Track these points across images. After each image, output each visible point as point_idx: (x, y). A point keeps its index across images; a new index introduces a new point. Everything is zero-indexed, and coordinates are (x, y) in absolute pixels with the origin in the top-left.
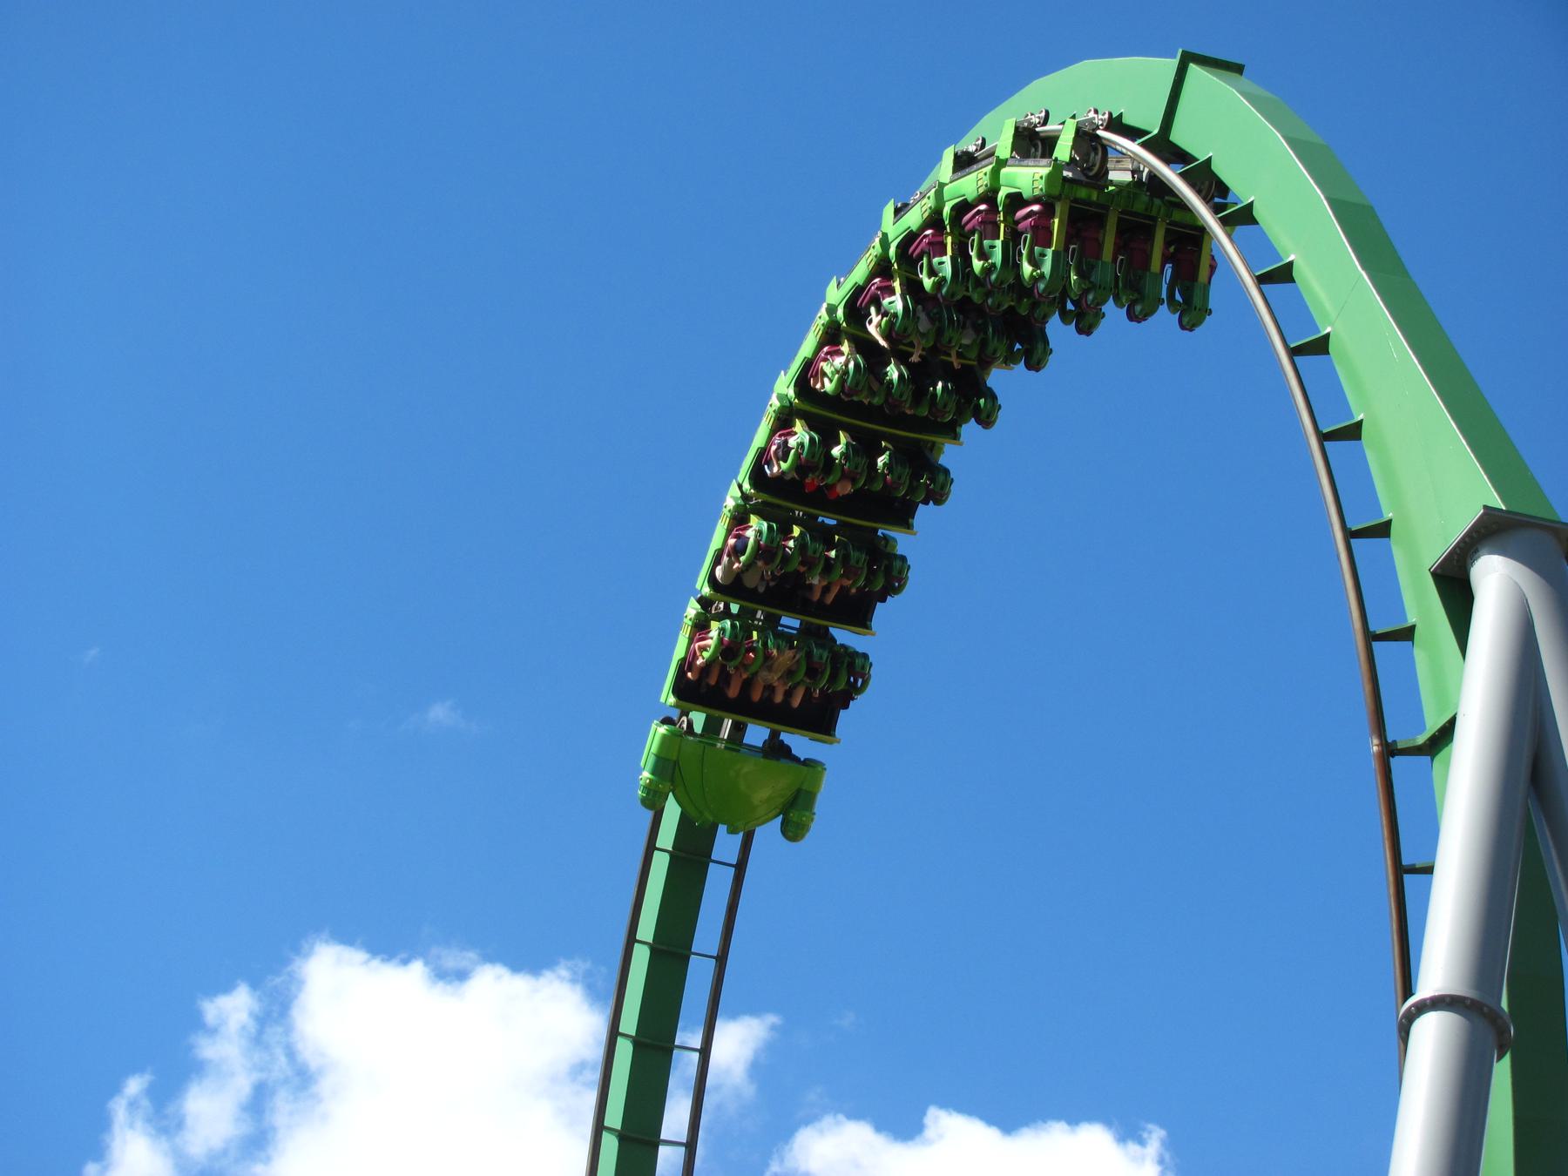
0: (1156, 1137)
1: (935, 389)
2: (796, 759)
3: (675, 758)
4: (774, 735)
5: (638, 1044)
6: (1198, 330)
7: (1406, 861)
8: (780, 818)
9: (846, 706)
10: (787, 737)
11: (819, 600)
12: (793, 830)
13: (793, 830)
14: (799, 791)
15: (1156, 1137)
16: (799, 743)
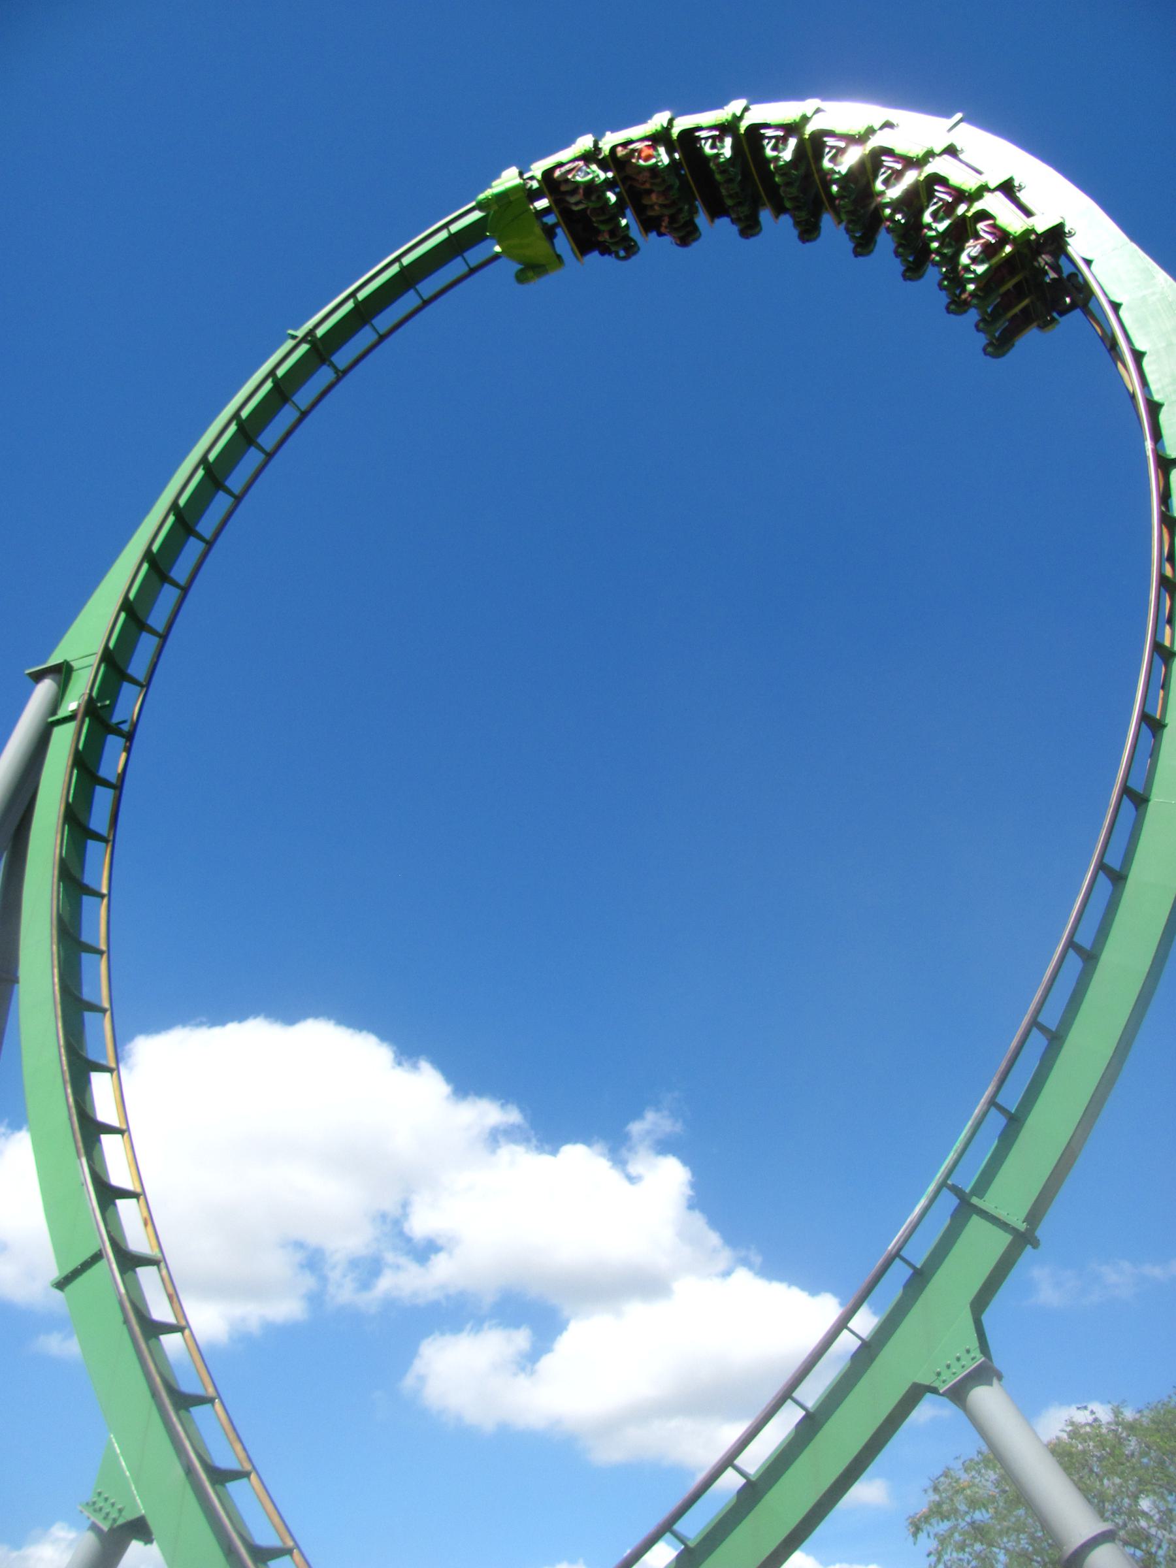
0: (581, 1561)
1: (794, 174)
2: (553, 244)
3: (512, 199)
4: (556, 225)
5: (358, 306)
6: (909, 283)
7: (902, 1253)
8: (521, 267)
9: (602, 254)
10: (559, 231)
11: (647, 205)
12: (521, 278)
13: (521, 278)
14: (543, 266)
15: (581, 1561)
16: (563, 242)
